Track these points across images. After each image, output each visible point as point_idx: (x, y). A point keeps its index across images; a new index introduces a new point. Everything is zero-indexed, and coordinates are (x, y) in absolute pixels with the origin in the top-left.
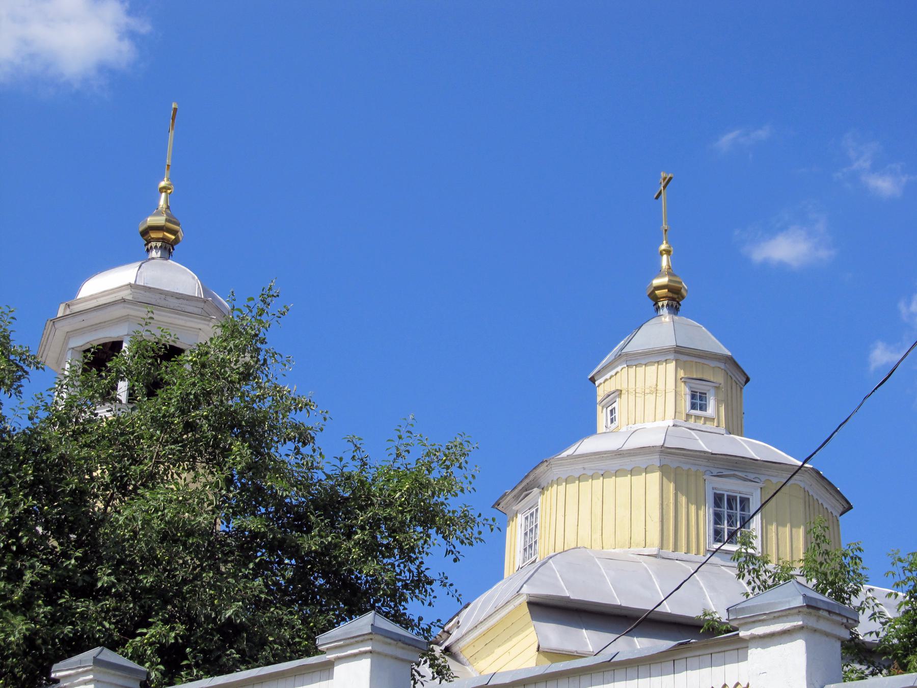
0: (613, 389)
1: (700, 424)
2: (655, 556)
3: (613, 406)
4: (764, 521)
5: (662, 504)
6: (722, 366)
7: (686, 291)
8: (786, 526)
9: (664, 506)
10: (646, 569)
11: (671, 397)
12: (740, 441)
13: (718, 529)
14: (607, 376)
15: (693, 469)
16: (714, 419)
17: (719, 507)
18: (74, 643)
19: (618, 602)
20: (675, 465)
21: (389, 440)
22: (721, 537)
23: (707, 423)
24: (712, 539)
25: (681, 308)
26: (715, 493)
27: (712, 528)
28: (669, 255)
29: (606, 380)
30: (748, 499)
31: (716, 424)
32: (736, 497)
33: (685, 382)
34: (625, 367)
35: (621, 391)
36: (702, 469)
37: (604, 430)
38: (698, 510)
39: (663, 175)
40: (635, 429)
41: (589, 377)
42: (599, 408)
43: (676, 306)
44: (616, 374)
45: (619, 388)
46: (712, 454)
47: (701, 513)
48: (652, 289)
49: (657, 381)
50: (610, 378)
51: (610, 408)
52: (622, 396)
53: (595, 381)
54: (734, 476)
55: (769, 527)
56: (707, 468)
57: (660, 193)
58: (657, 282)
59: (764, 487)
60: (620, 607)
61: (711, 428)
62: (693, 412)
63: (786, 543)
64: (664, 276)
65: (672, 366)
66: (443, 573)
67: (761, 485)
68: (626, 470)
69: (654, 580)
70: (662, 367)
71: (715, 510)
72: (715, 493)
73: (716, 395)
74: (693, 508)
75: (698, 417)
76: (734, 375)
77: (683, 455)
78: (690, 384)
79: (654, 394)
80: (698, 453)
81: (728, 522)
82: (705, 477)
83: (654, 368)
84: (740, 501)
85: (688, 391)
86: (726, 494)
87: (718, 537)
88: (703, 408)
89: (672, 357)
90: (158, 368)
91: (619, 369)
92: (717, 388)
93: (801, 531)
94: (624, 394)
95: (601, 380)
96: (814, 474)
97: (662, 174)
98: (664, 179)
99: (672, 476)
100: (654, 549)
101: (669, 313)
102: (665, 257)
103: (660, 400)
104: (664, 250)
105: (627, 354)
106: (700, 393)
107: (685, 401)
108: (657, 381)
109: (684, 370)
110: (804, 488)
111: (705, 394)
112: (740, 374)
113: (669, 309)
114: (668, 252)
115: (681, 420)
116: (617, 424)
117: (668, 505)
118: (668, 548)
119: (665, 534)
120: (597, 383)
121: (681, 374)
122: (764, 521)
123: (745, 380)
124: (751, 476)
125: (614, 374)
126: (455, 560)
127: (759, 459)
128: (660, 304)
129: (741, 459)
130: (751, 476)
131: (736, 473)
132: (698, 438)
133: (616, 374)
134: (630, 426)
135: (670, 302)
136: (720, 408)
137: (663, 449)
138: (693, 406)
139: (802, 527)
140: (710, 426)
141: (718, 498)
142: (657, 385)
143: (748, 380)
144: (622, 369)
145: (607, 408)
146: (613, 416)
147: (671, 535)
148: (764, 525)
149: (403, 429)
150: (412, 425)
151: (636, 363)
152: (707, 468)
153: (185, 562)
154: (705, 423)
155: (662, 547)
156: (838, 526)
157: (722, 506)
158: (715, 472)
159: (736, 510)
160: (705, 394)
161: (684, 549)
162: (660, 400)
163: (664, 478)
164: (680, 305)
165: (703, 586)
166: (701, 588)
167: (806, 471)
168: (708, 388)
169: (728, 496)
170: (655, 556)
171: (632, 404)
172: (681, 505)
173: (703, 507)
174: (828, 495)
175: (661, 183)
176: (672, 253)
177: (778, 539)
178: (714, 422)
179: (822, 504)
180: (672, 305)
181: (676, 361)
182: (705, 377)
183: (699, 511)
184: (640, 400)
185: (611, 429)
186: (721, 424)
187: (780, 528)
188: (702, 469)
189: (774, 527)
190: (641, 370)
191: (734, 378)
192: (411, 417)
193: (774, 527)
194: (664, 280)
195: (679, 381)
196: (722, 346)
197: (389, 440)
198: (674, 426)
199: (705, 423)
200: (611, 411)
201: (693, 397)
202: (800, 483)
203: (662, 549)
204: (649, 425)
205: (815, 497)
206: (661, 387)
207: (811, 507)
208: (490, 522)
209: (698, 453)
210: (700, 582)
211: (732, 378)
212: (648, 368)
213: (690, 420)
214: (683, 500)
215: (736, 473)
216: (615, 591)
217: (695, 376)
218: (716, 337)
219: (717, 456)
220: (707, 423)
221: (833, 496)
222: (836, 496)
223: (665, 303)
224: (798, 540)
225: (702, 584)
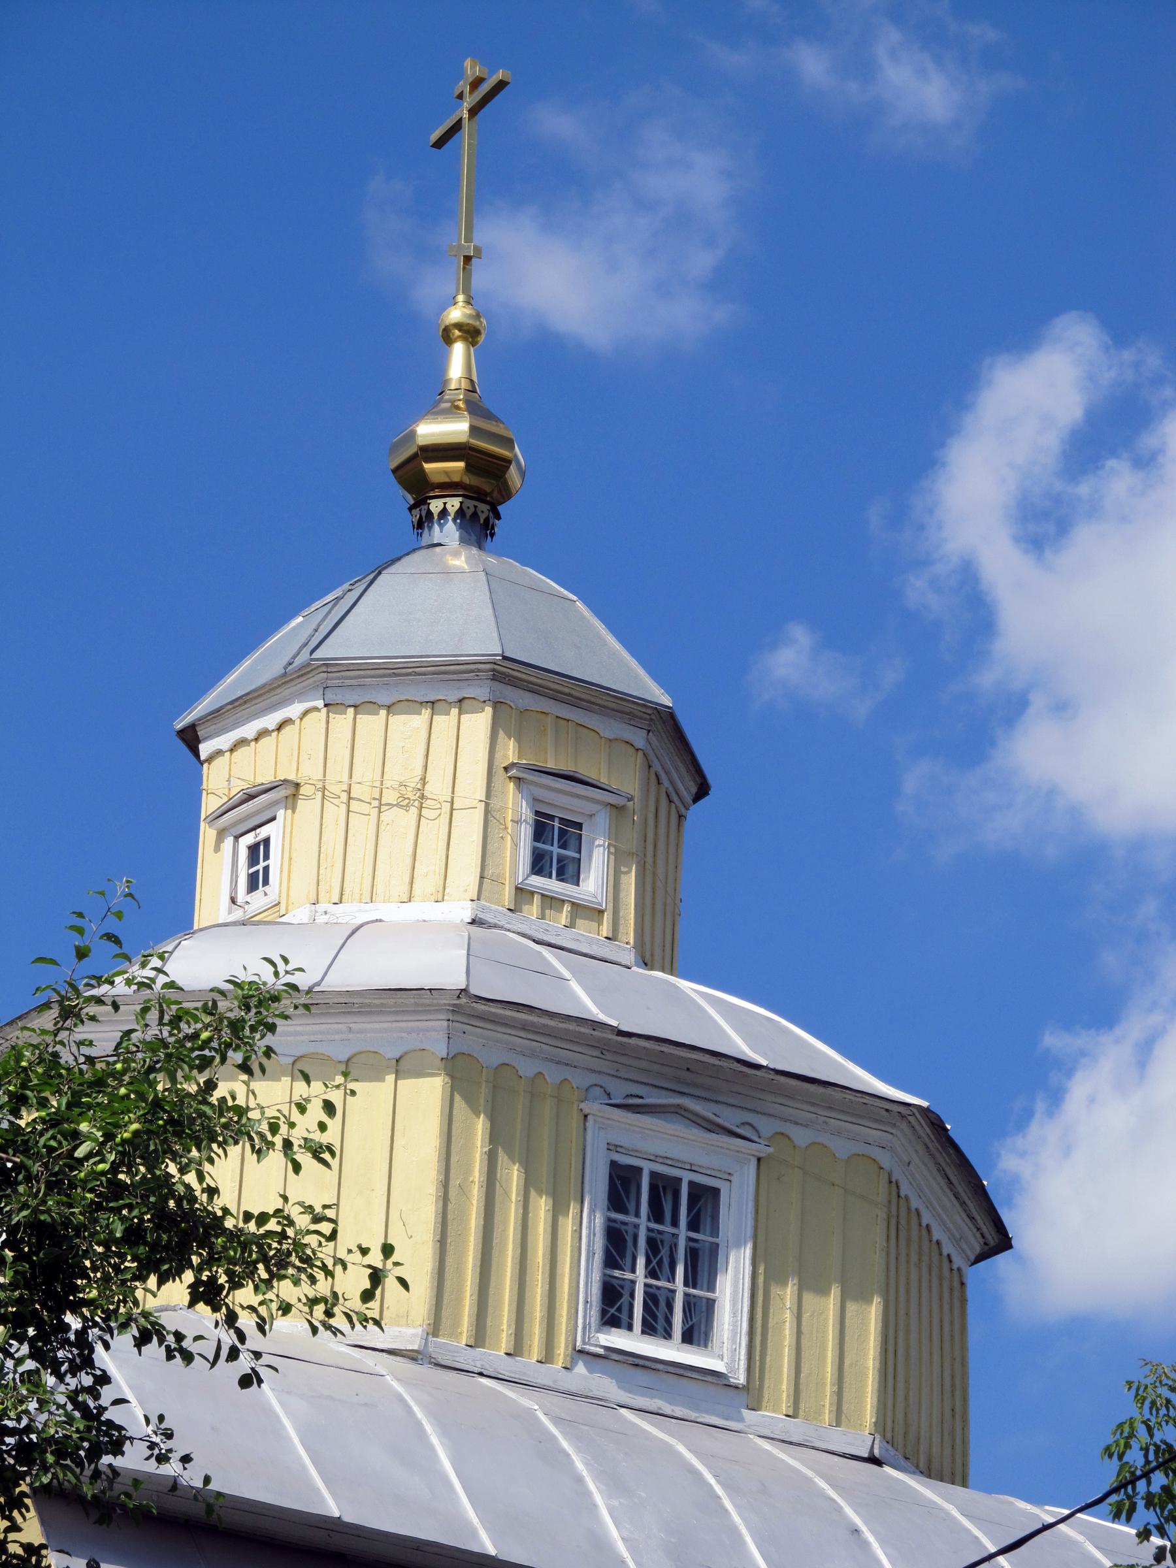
0: (266, 777)
1: (557, 924)
2: (412, 1356)
3: (263, 832)
4: (761, 1270)
5: (445, 1184)
6: (639, 738)
7: (523, 474)
8: (869, 1301)
9: (453, 1193)
10: (401, 1399)
11: (470, 825)
12: (693, 995)
13: (614, 1282)
14: (249, 730)
15: (553, 1075)
16: (601, 912)
17: (622, 1209)
19: (332, 1508)
20: (492, 1058)
21: (40, 960)
22: (619, 1310)
23: (579, 922)
24: (595, 1313)
25: (500, 527)
26: (613, 1164)
27: (596, 1277)
28: (473, 344)
29: (242, 742)
30: (716, 1192)
31: (605, 930)
32: (679, 1180)
33: (518, 780)
34: (316, 709)
35: (297, 785)
36: (580, 1080)
37: (223, 914)
38: (557, 1211)
39: (471, 69)
40: (360, 922)
41: (179, 725)
42: (207, 834)
43: (487, 520)
44: (279, 728)
45: (292, 777)
46: (621, 1033)
47: (568, 1225)
48: (413, 450)
49: (426, 767)
50: (256, 740)
51: (249, 839)
52: (301, 804)
54: (678, 1112)
55: (775, 1290)
56: (594, 1079)
57: (457, 127)
58: (430, 431)
59: (769, 1156)
60: (334, 1526)
61: (590, 942)
62: (537, 881)
63: (823, 1348)
64: (452, 411)
65: (479, 722)
66: (161, 1418)
67: (761, 1149)
68: (329, 1058)
69: (435, 1440)
70: (445, 722)
71: (609, 1220)
72: (613, 1164)
73: (614, 835)
74: (542, 1206)
75: (551, 902)
76: (667, 773)
77: (525, 1027)
78: (532, 788)
79: (414, 811)
80: (571, 1026)
81: (648, 1262)
82: (587, 1107)
83: (417, 722)
84: (690, 1195)
85: (527, 814)
86: (647, 1167)
87: (612, 1311)
88: (569, 871)
89: (481, 690)
91: (293, 710)
92: (618, 810)
93: (873, 1312)
94: (308, 798)
95: (223, 742)
96: (925, 1130)
97: (468, 63)
98: (476, 83)
99: (484, 1092)
100: (411, 1331)
101: (462, 540)
102: (458, 350)
103: (433, 832)
104: (458, 326)
105: (328, 665)
106: (563, 821)
107: (515, 845)
108: (426, 767)
109: (519, 741)
110: (890, 1175)
111: (579, 826)
112: (683, 769)
113: (461, 527)
114: (470, 333)
115: (496, 911)
116: (273, 897)
117: (464, 1190)
118: (454, 1334)
119: (448, 1285)
120: (205, 749)
121: (510, 752)
122: (761, 1270)
123: (694, 790)
124: (729, 1117)
126: (246, 1381)
127: (764, 1062)
128: (436, 506)
129: (736, 1065)
130: (729, 1117)
131: (687, 1102)
132: (566, 974)
133: (279, 728)
134: (321, 907)
135: (470, 503)
136: (624, 878)
137: (463, 1000)
138: (539, 864)
139: (877, 1301)
140: (588, 935)
141: (619, 1177)
142: (424, 780)
143: (703, 790)
144: (306, 713)
145: (237, 838)
146: (260, 867)
147: (468, 1294)
148: (761, 1279)
149: (93, 928)
150: (119, 915)
151: (355, 698)
152: (594, 1079)
154: (571, 925)
155: (435, 1329)
156: (964, 1301)
157: (631, 1207)
158: (620, 1091)
159: (675, 1223)
160: (579, 826)
161: (505, 1341)
162: (433, 832)
163: (457, 1098)
164: (498, 517)
165: (585, 1473)
166: (580, 1480)
167: (902, 1116)
168: (590, 807)
169: (654, 1175)
170: (412, 1356)
171: (334, 835)
172: (507, 1194)
173: (573, 1208)
174: (949, 1201)
175: (460, 96)
176: (482, 339)
177: (799, 1333)
178: (600, 923)
179: (928, 1226)
180: (475, 515)
181: (497, 705)
183: (561, 1219)
184: (362, 827)
185: (251, 909)
186: (622, 929)
187: (851, 1307)
188: (580, 1080)
189: (789, 1292)
190: (371, 724)
192: (121, 888)
193: (789, 1292)
194: (455, 429)
195: (500, 775)
196: (641, 672)
197: (40, 960)
198: (473, 922)
199: (571, 925)
200: (253, 850)
201: (540, 830)
202: (877, 1153)
203: (435, 1334)
204: (391, 912)
205: (915, 1203)
206: (438, 787)
207: (902, 1235)
208: (375, 1258)
209: (571, 1026)
210: (574, 1457)
212: (397, 721)
213: (525, 908)
214: (513, 1175)
215: (687, 1102)
216: (315, 1464)
217: (551, 765)
218: (621, 640)
219: (633, 1041)
220: (579, 922)
221: (963, 1204)
222: (971, 1206)
223: (454, 504)
224: (862, 1339)
225: (580, 1466)
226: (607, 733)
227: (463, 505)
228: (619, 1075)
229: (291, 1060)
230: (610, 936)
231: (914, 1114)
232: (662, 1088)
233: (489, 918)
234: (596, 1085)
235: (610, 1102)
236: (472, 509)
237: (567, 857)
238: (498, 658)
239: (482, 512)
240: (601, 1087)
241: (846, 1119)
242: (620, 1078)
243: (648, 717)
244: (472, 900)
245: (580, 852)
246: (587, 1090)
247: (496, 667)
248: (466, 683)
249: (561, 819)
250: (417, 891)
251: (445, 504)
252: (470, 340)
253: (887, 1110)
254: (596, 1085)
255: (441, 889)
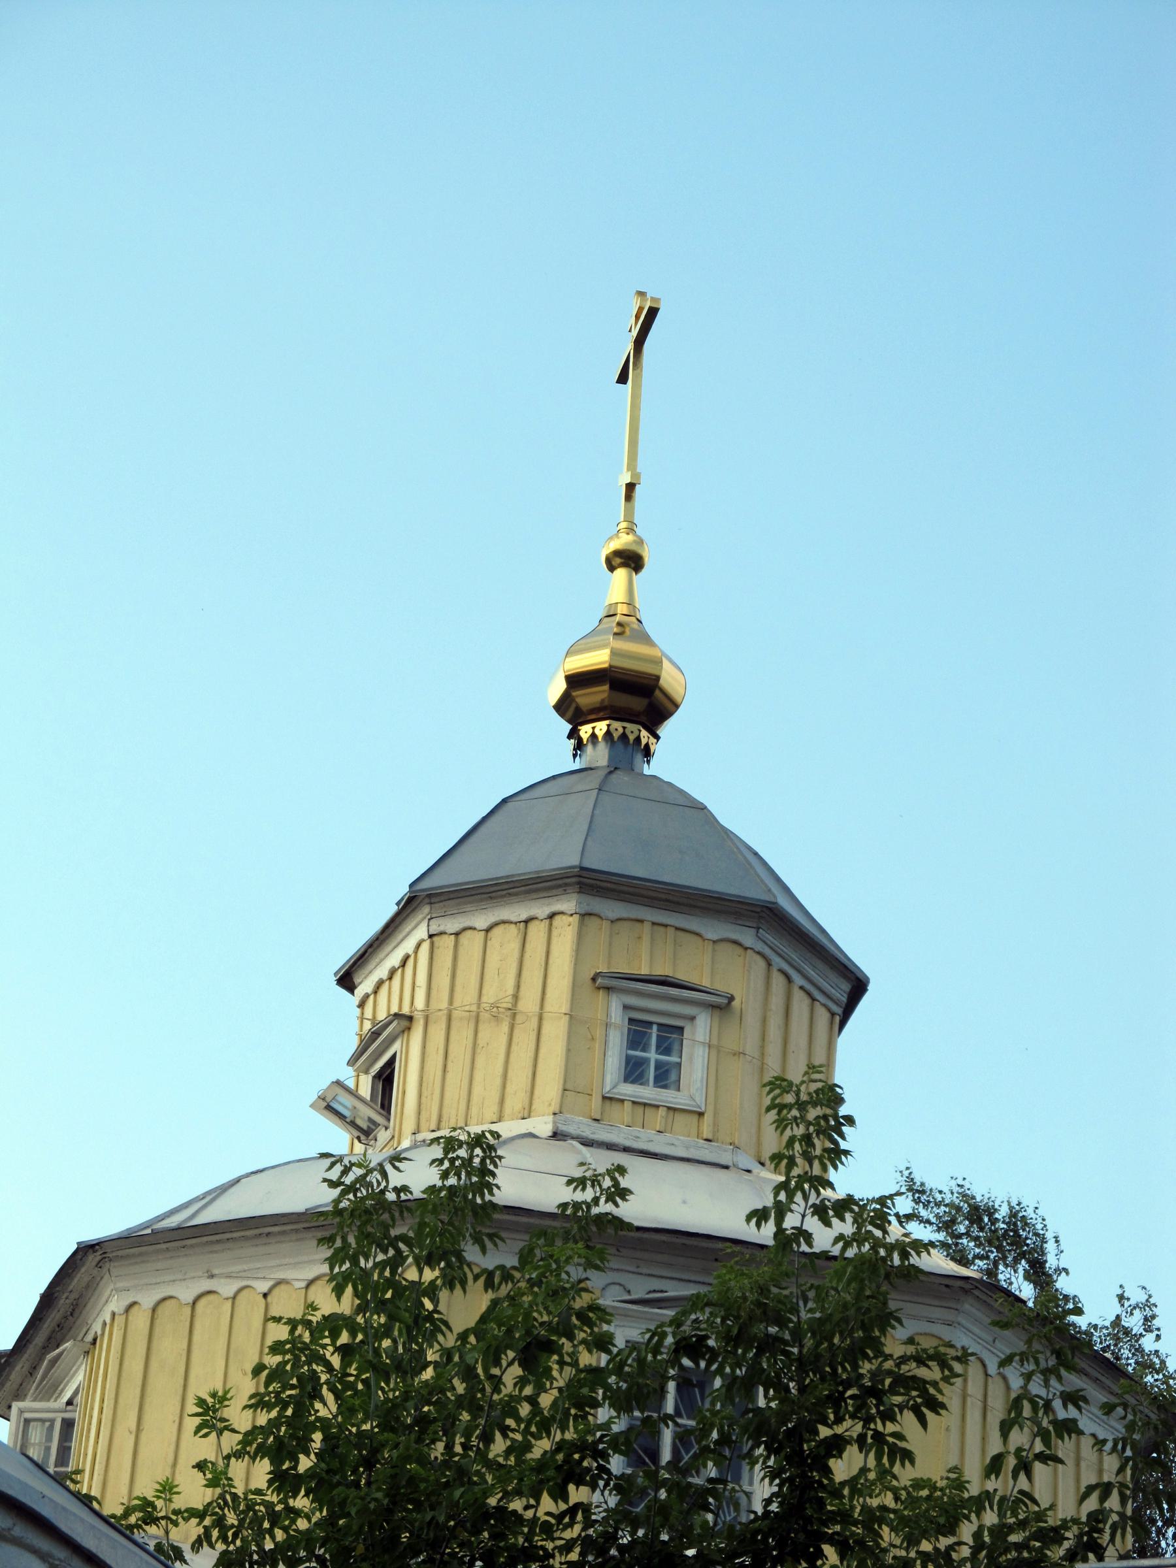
11: (556, 1032)
18: (812, 1550)
53: (355, 987)
62: (629, 1090)
65: (566, 932)
88: (665, 1076)
90: (942, 1198)
123: (846, 987)
125: (397, 964)
135: (618, 726)
138: (633, 1071)
142: (516, 997)
143: (858, 986)
153: (356, 1484)
182: (682, 975)
191: (798, 980)
201: (637, 1034)
206: (529, 1003)
211: (789, 979)
226: (711, 935)
227: (611, 727)
228: (640, 1272)
229: (303, 1284)
230: (710, 1137)
231: (977, 1287)
232: (690, 1281)
233: (571, 1129)
234: (614, 1283)
235: (627, 1297)
236: (621, 730)
237: (668, 1063)
238: (576, 870)
239: (632, 732)
240: (620, 1285)
241: (670, 1275)
242: (641, 1274)
243: (756, 915)
244: (555, 1114)
245: (681, 1057)
246: (603, 1289)
247: (582, 879)
248: (555, 898)
249: (660, 1025)
250: (508, 1110)
251: (594, 728)
252: (633, 565)
253: (947, 1286)
254: (614, 1283)
255: (527, 1107)
